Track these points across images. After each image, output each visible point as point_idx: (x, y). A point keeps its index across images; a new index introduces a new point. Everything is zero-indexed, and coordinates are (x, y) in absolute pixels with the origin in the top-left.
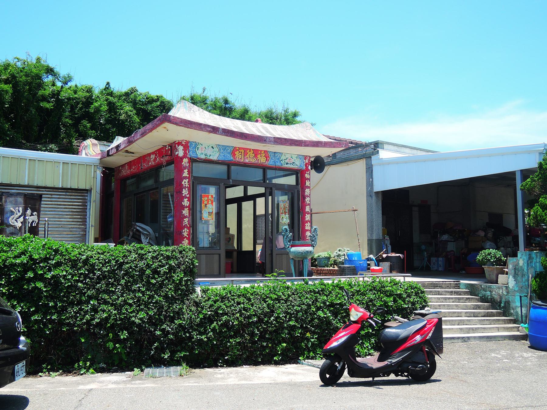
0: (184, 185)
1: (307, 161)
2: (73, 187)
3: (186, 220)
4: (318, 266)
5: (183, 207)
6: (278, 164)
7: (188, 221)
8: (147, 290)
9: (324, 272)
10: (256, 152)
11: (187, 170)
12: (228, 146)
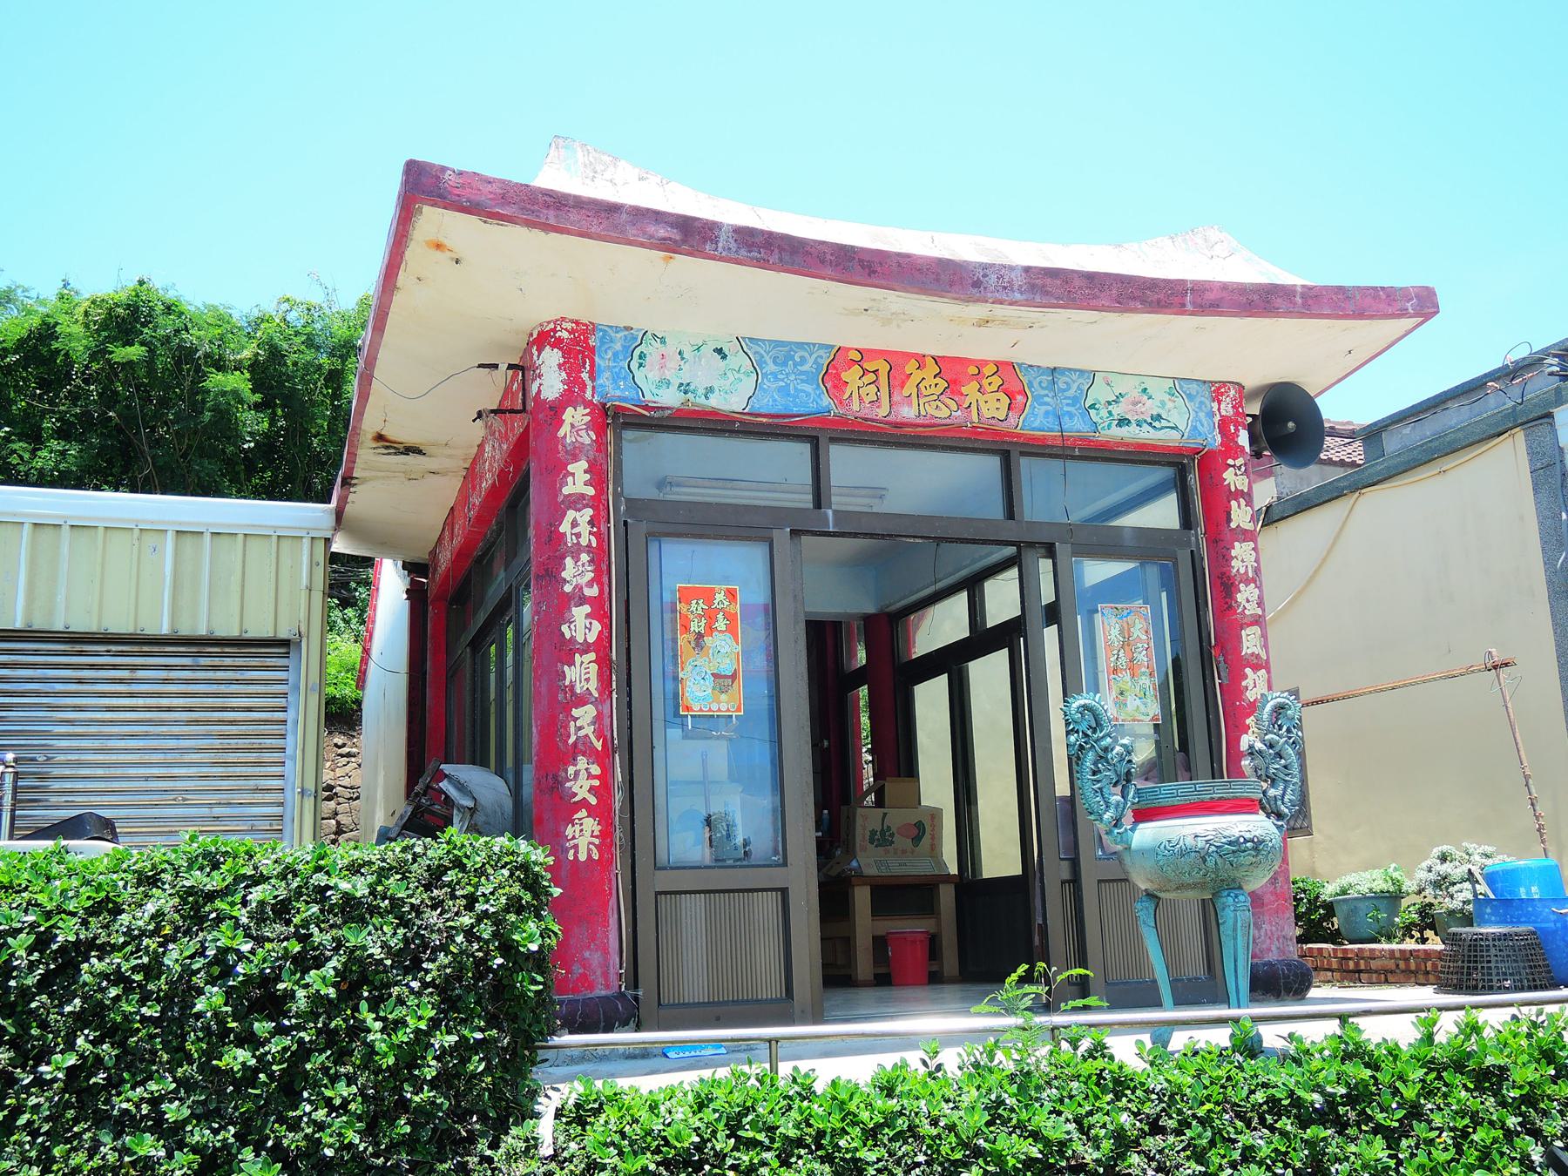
0: (570, 540)
1: (1227, 409)
2: (221, 633)
3: (585, 715)
4: (1327, 939)
5: (567, 651)
6: (1076, 426)
7: (598, 718)
8: (203, 1116)
9: (1374, 964)
10: (954, 372)
11: (583, 464)
12: (801, 345)
